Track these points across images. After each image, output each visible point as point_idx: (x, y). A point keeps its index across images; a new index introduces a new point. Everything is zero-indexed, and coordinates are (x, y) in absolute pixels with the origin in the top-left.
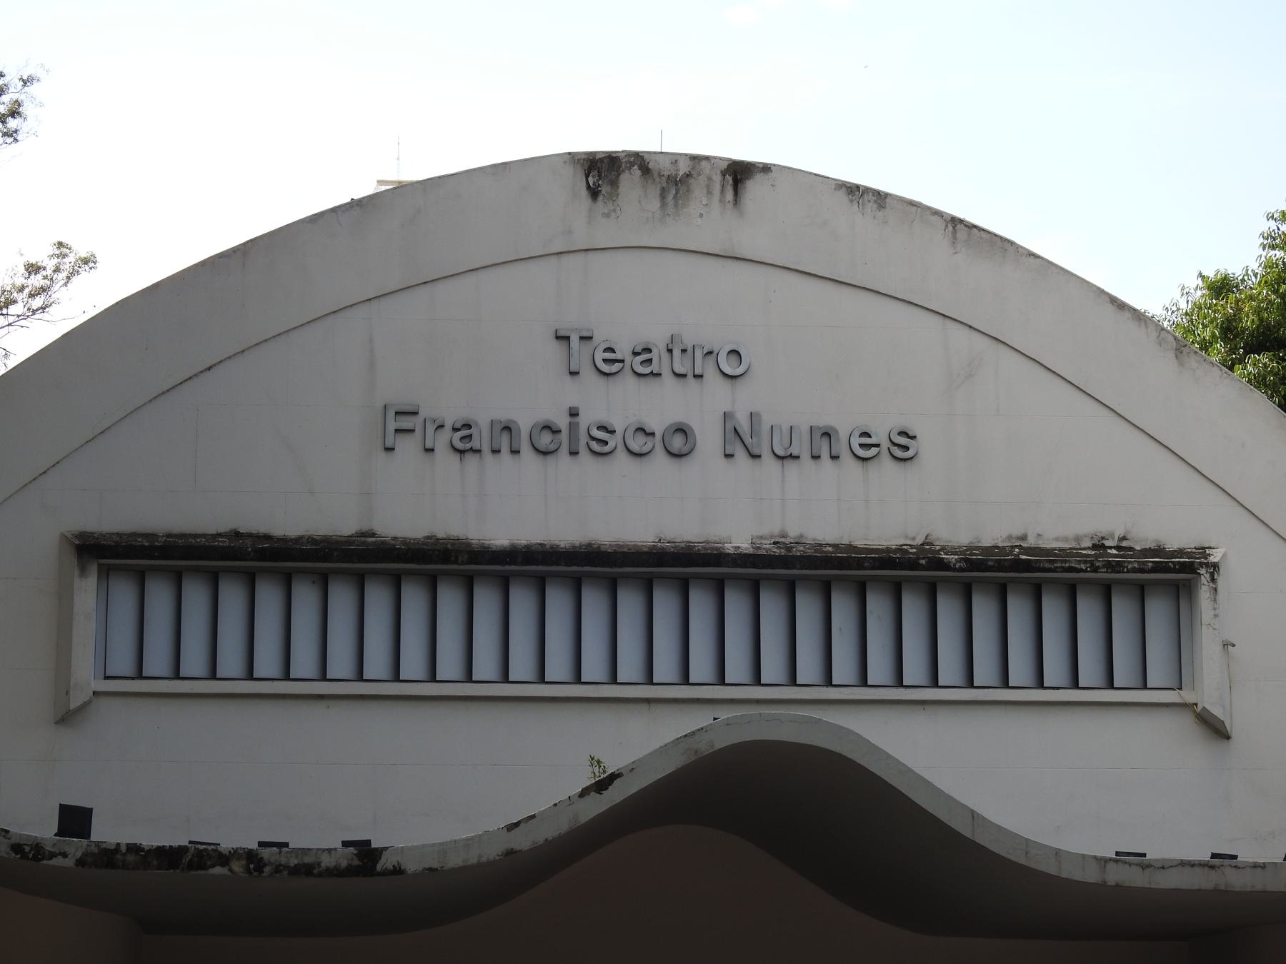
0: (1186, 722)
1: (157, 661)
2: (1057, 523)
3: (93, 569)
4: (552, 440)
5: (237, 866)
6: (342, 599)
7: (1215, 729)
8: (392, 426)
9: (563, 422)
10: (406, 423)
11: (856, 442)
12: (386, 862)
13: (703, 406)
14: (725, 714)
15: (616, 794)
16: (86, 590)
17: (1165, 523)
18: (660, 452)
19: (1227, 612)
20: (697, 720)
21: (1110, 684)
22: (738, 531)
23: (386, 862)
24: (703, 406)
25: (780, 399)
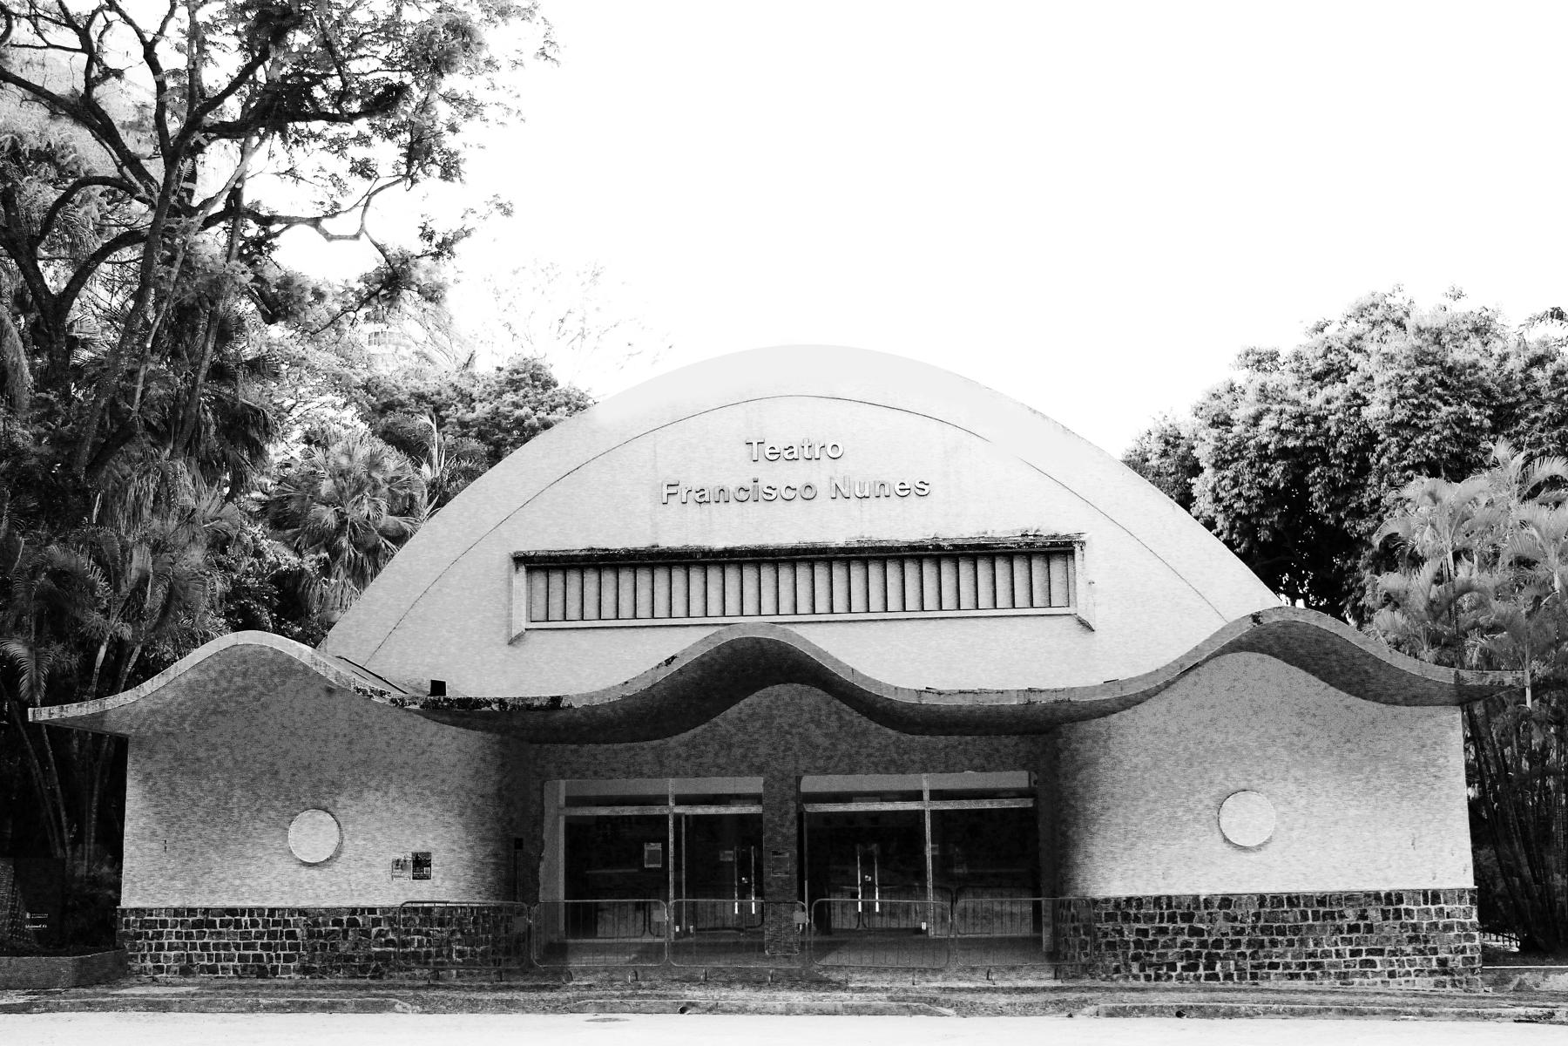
0: (1072, 622)
1: (556, 612)
2: (1003, 526)
3: (522, 569)
4: (748, 494)
5: (495, 707)
6: (983, 568)
7: (1087, 626)
8: (666, 491)
9: (749, 485)
10: (673, 490)
11: (898, 487)
12: (564, 703)
13: (820, 475)
14: (715, 630)
15: (675, 667)
16: (520, 578)
17: (1053, 523)
18: (798, 498)
19: (1087, 564)
20: (697, 635)
21: (1042, 606)
22: (838, 537)
23: (564, 703)
24: (820, 475)
25: (857, 468)
